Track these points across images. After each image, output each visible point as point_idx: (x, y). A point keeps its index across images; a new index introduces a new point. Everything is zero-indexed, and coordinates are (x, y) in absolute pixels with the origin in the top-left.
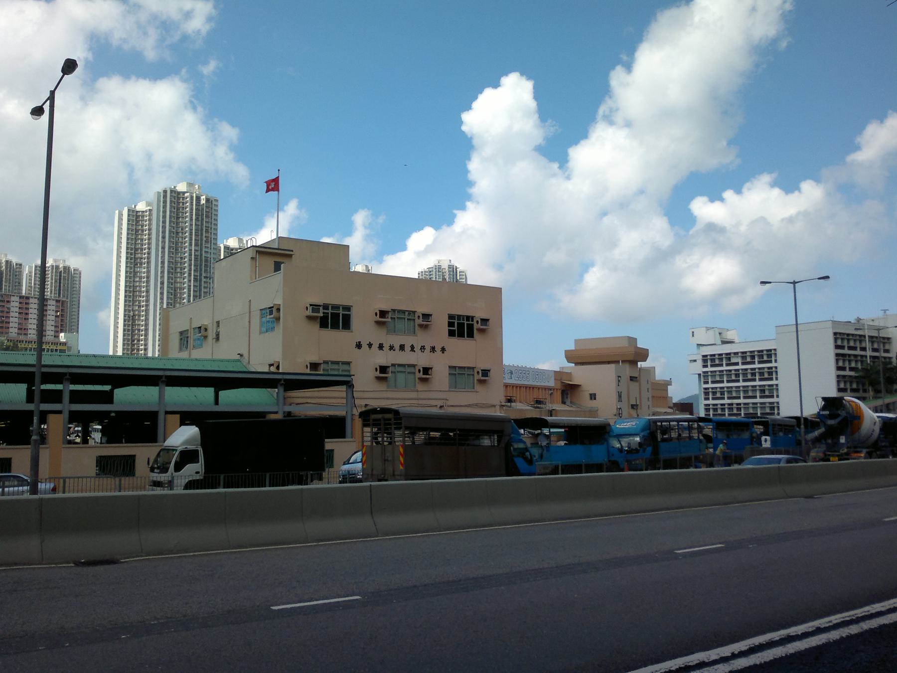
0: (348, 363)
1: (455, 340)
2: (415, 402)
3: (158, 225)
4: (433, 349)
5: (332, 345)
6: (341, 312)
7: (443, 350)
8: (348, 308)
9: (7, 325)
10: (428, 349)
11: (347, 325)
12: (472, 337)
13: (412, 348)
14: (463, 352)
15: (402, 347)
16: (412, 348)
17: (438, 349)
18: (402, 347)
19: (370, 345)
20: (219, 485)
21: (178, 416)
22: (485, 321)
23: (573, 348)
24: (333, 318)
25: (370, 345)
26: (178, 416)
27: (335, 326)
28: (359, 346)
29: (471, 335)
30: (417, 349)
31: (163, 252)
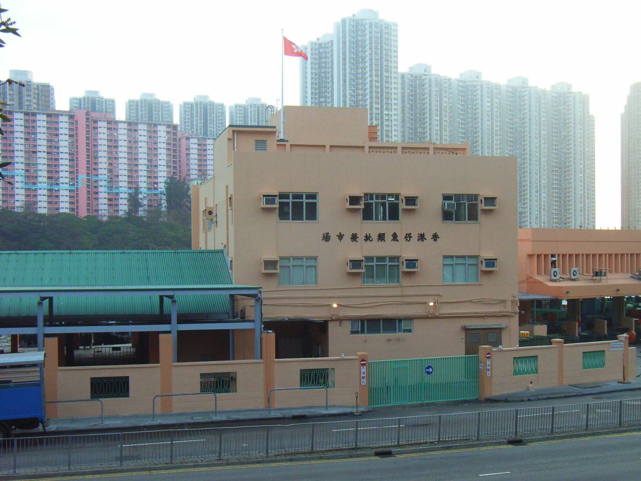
0: (315, 258)
1: (452, 225)
2: (399, 299)
3: (338, 57)
4: (422, 237)
5: (296, 237)
6: (305, 200)
7: (435, 237)
8: (313, 196)
9: (156, 181)
10: (415, 237)
11: (312, 214)
12: (476, 219)
13: (395, 237)
14: (462, 237)
15: (381, 237)
16: (395, 237)
17: (429, 236)
18: (381, 237)
19: (341, 237)
20: (395, 330)
21: (56, 339)
22: (490, 200)
23: (619, 228)
24: (297, 207)
25: (341, 237)
26: (56, 339)
27: (297, 216)
28: (326, 238)
29: (473, 217)
30: (401, 237)
31: (344, 85)
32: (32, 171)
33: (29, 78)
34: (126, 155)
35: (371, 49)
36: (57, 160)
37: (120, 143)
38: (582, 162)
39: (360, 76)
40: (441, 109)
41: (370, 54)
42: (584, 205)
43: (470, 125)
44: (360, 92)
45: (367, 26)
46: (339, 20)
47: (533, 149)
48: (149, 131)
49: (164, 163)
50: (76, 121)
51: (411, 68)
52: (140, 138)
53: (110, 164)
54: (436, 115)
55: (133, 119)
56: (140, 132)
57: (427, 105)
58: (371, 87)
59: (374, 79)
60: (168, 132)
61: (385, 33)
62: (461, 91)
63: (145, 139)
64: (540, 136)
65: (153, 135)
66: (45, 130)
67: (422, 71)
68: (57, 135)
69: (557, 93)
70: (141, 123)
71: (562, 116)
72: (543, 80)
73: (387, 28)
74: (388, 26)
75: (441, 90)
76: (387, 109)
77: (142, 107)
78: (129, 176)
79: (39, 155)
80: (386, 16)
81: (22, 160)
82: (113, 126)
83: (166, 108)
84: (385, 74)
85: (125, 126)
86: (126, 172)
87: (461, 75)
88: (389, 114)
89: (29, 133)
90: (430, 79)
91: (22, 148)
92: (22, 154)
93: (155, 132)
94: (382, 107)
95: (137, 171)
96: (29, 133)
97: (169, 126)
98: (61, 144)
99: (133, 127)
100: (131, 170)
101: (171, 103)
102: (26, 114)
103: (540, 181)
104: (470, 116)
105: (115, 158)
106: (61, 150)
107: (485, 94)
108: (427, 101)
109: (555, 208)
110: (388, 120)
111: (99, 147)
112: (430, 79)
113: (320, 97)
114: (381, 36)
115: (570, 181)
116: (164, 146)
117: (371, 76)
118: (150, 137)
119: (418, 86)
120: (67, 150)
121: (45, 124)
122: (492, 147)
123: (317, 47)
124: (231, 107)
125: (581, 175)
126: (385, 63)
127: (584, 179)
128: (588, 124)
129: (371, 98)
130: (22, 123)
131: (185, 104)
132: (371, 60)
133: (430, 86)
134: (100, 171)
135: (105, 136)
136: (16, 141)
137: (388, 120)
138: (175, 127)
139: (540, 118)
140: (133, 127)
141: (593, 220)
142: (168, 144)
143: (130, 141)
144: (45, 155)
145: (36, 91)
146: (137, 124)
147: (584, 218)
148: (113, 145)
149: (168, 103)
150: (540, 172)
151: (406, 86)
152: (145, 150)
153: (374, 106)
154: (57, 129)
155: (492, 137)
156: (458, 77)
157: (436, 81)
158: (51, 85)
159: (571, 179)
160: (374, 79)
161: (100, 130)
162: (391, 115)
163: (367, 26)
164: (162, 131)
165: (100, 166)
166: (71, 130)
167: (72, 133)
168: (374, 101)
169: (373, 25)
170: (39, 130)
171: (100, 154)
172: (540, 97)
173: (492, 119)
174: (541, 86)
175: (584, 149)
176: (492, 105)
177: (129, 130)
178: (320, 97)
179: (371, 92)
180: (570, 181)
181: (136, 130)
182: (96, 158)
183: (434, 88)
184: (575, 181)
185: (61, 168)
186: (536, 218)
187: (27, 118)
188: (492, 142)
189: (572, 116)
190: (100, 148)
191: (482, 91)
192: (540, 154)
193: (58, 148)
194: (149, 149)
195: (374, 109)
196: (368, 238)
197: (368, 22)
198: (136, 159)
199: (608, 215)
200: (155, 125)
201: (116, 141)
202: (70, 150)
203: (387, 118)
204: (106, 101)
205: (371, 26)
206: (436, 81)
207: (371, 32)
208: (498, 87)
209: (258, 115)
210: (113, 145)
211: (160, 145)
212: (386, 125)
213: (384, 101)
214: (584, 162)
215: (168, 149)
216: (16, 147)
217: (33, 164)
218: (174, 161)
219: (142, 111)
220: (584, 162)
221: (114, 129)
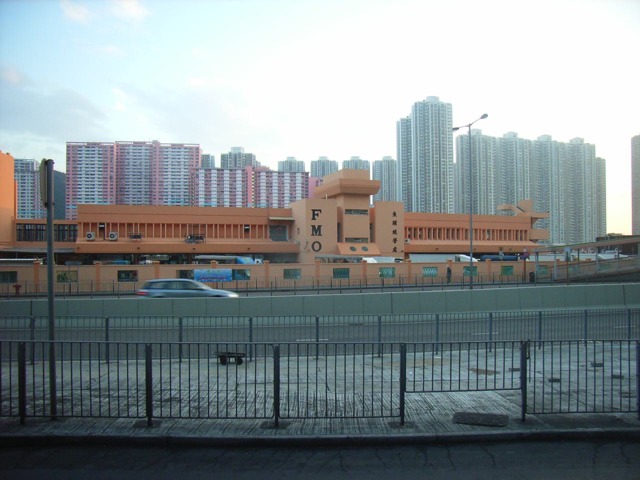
32: (221, 202)
33: (295, 159)
34: (277, 191)
35: (432, 120)
36: (235, 195)
37: (274, 184)
38: (590, 190)
39: (426, 138)
40: (486, 157)
41: (432, 124)
42: (592, 219)
43: (509, 167)
44: (426, 148)
45: (430, 107)
46: (414, 104)
47: (554, 182)
48: (291, 177)
49: (300, 195)
50: (247, 173)
51: (538, 138)
52: (285, 181)
53: (268, 197)
54: (436, 154)
55: (281, 170)
56: (285, 178)
57: (477, 155)
58: (432, 144)
59: (434, 139)
60: (302, 177)
61: (442, 110)
62: (503, 145)
63: (289, 181)
64: (558, 173)
65: (293, 179)
66: (228, 179)
67: (546, 140)
68: (235, 181)
69: (572, 145)
70: (286, 172)
71: (576, 160)
72: (563, 136)
73: (442, 107)
74: (443, 106)
75: (486, 145)
76: (444, 158)
77: (318, 165)
78: (278, 204)
79: (225, 193)
80: (444, 100)
81: (216, 196)
82: (269, 175)
83: (301, 164)
84: (442, 136)
85: (277, 174)
86: (277, 202)
87: (504, 135)
88: (444, 161)
89: (219, 181)
90: (479, 138)
91: (216, 189)
92: (216, 193)
93: (295, 177)
94: (440, 156)
95: (283, 201)
96: (219, 181)
97: (303, 173)
98: (237, 186)
99: (281, 175)
100: (280, 200)
101: (336, 161)
102: (230, 170)
103: (559, 203)
104: (509, 161)
105: (270, 193)
106: (237, 189)
107: (518, 147)
108: (477, 152)
109: (572, 220)
110: (444, 165)
111: (261, 187)
112: (479, 138)
113: (407, 153)
114: (439, 113)
115: (582, 202)
116: (300, 185)
117: (432, 137)
118: (292, 180)
119: (472, 145)
120: (241, 190)
121: (228, 175)
122: (524, 181)
123: (405, 122)
124: (373, 162)
125: (589, 199)
126: (441, 129)
127: (592, 201)
128: (600, 166)
129: (433, 151)
130: (216, 175)
131: (344, 162)
132: (432, 127)
133: (479, 143)
134: (261, 202)
135: (265, 181)
136: (212, 186)
137: (444, 165)
138: (307, 174)
139: (558, 161)
140: (281, 175)
141: (68, 149)
142: (302, 184)
143: (279, 183)
144: (228, 193)
145: (245, 158)
146: (283, 173)
147: (592, 227)
148: (269, 186)
149: (334, 162)
150: (559, 197)
151: (464, 143)
152: (289, 188)
153: (435, 156)
154: (235, 178)
155: (524, 175)
156: (569, 142)
157: (483, 139)
158: (253, 154)
159: (583, 201)
160: (434, 139)
161: (262, 177)
162: (447, 162)
163: (430, 107)
164: (299, 177)
165: (261, 198)
166: (243, 178)
167: (244, 180)
168: (434, 153)
169: (433, 105)
170: (225, 179)
171: (261, 191)
172: (558, 147)
173: (523, 163)
174: (559, 140)
175: (592, 181)
176: (523, 154)
177: (279, 176)
178: (407, 153)
179: (433, 148)
180: (582, 202)
181: (283, 177)
182: (259, 193)
183: (482, 144)
184: (585, 202)
185: (237, 200)
186: (556, 227)
187: (219, 172)
188: (524, 178)
189: (583, 159)
190: (261, 188)
191: (516, 145)
192: (559, 185)
193: (236, 188)
194: (291, 187)
195: (435, 158)
196: (395, 232)
197: (430, 104)
198: (283, 194)
199: (618, 222)
200: (295, 173)
201: (271, 183)
202: (242, 189)
203: (443, 163)
204: (298, 162)
205: (432, 106)
206: (483, 139)
207: (432, 110)
208: (562, 144)
209: (389, 166)
210: (269, 186)
211: (297, 185)
212: (443, 168)
213: (442, 153)
214: (592, 190)
215: (302, 187)
216: (212, 189)
217: (222, 199)
218: (306, 194)
219: (318, 167)
220: (592, 190)
221: (270, 176)
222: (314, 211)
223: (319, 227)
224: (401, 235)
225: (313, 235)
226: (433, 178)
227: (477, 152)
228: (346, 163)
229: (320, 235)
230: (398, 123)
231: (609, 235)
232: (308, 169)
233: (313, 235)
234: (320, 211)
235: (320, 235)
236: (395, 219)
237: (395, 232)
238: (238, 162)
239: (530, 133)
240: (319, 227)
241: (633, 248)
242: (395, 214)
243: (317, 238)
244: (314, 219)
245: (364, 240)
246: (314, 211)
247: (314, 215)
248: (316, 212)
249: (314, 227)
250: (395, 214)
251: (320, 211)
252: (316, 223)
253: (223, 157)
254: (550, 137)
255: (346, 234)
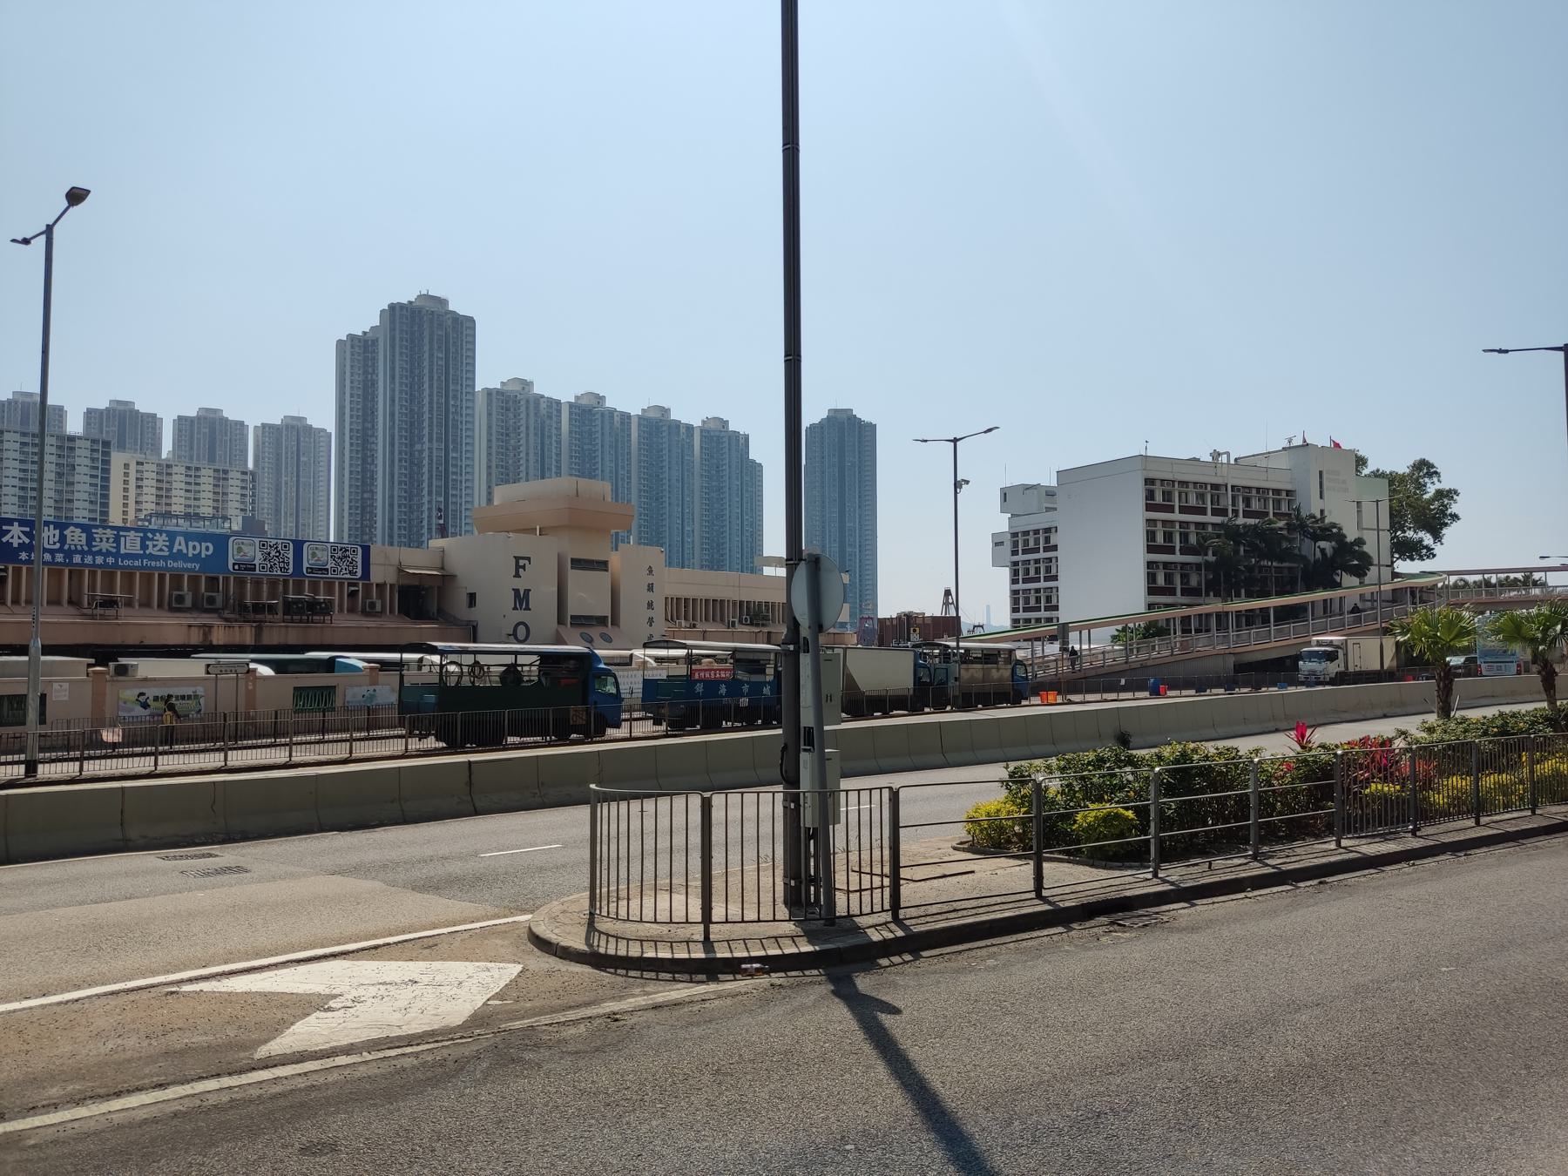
149: (154, 416)
222: (517, 559)
223: (527, 591)
224: (659, 612)
225: (515, 608)
226: (430, 478)
227: (599, 441)
228: (91, 415)
229: (528, 608)
230: (339, 342)
231: (1498, 592)
232: (75, 425)
233: (515, 608)
234: (529, 559)
235: (528, 608)
236: (650, 579)
237: (650, 605)
238: (209, 434)
239: (628, 398)
240: (527, 591)
241: (104, 734)
242: (650, 571)
243: (521, 615)
244: (517, 575)
245: (601, 621)
246: (517, 559)
247: (518, 567)
248: (522, 562)
249: (517, 591)
250: (650, 571)
251: (529, 559)
252: (521, 585)
253: (90, 414)
254: (667, 411)
255: (573, 609)
